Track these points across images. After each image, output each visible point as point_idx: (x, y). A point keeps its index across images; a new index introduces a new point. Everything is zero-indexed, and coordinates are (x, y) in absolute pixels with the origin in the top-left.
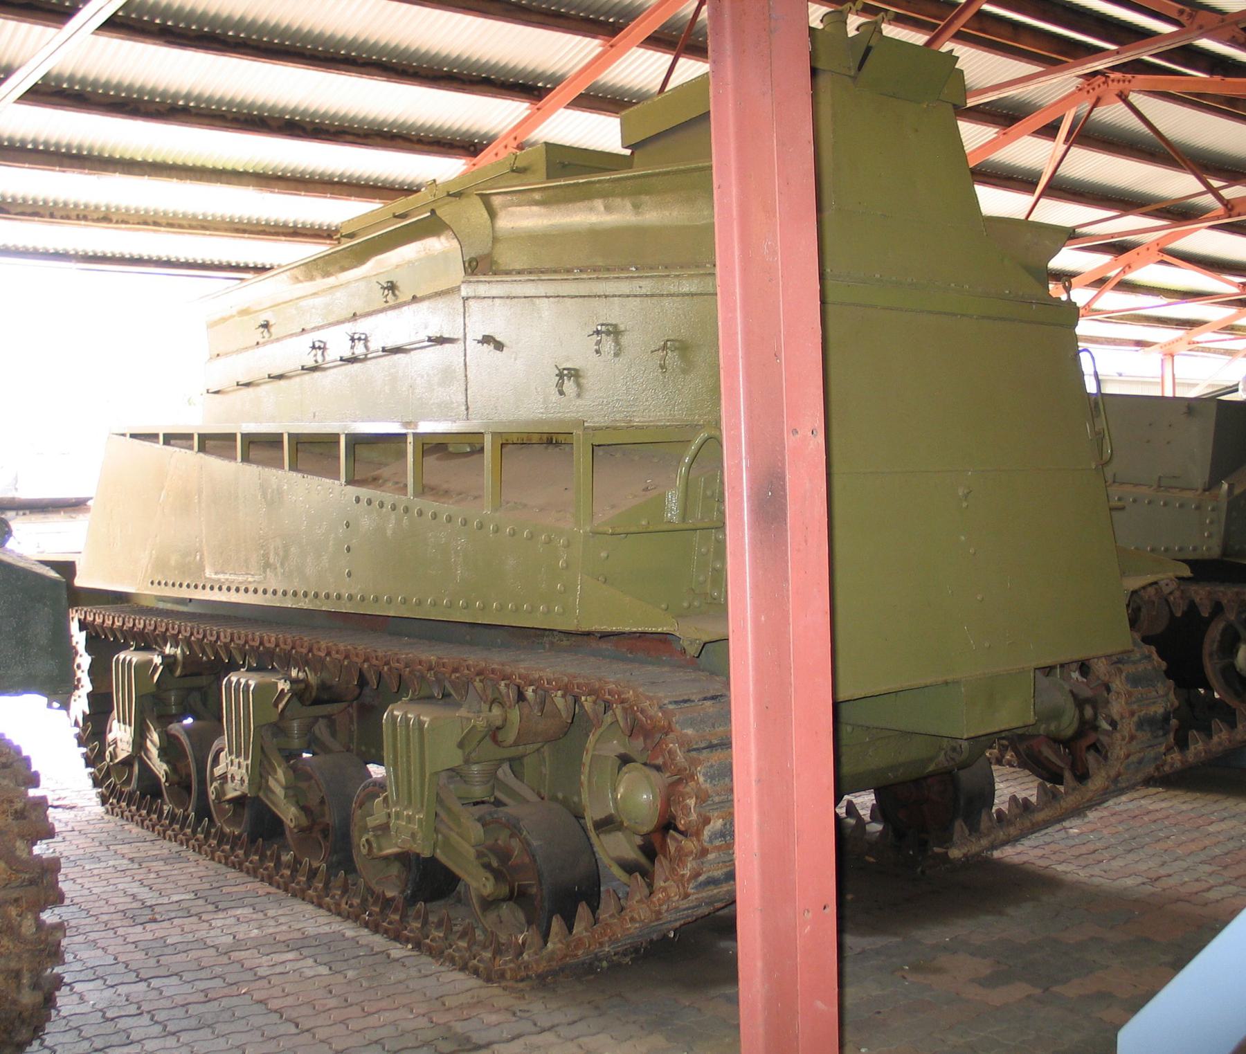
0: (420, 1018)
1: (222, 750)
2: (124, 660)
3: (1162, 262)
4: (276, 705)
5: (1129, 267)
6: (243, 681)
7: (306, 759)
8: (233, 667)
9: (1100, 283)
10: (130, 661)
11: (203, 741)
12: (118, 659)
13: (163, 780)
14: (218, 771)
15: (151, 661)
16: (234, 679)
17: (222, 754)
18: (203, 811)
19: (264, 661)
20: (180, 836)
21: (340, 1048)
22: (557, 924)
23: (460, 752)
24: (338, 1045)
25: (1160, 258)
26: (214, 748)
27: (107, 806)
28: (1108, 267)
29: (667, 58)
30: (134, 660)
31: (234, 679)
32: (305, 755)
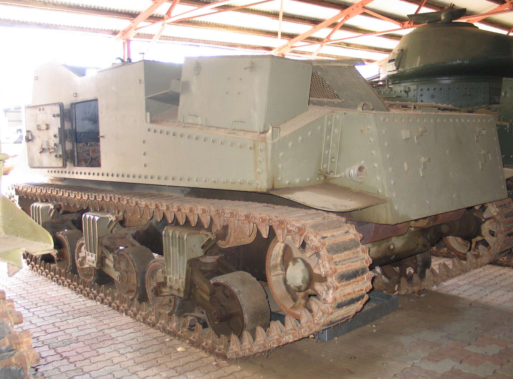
0: (131, 360)
1: (82, 245)
2: (36, 207)
3: (364, 14)
4: (108, 227)
5: (348, 16)
6: (92, 217)
7: (121, 249)
8: (87, 210)
9: (334, 25)
10: (39, 208)
11: (73, 240)
12: (33, 206)
13: (56, 257)
14: (81, 255)
15: (49, 207)
16: (88, 216)
17: (83, 248)
18: (74, 270)
19: (45, 199)
20: (60, 281)
21: (119, 377)
22: (260, 330)
23: (202, 250)
24: (117, 375)
25: (362, 11)
26: (78, 245)
27: (30, 265)
28: (338, 17)
29: (418, 7)
30: (41, 207)
31: (88, 216)
32: (121, 248)
